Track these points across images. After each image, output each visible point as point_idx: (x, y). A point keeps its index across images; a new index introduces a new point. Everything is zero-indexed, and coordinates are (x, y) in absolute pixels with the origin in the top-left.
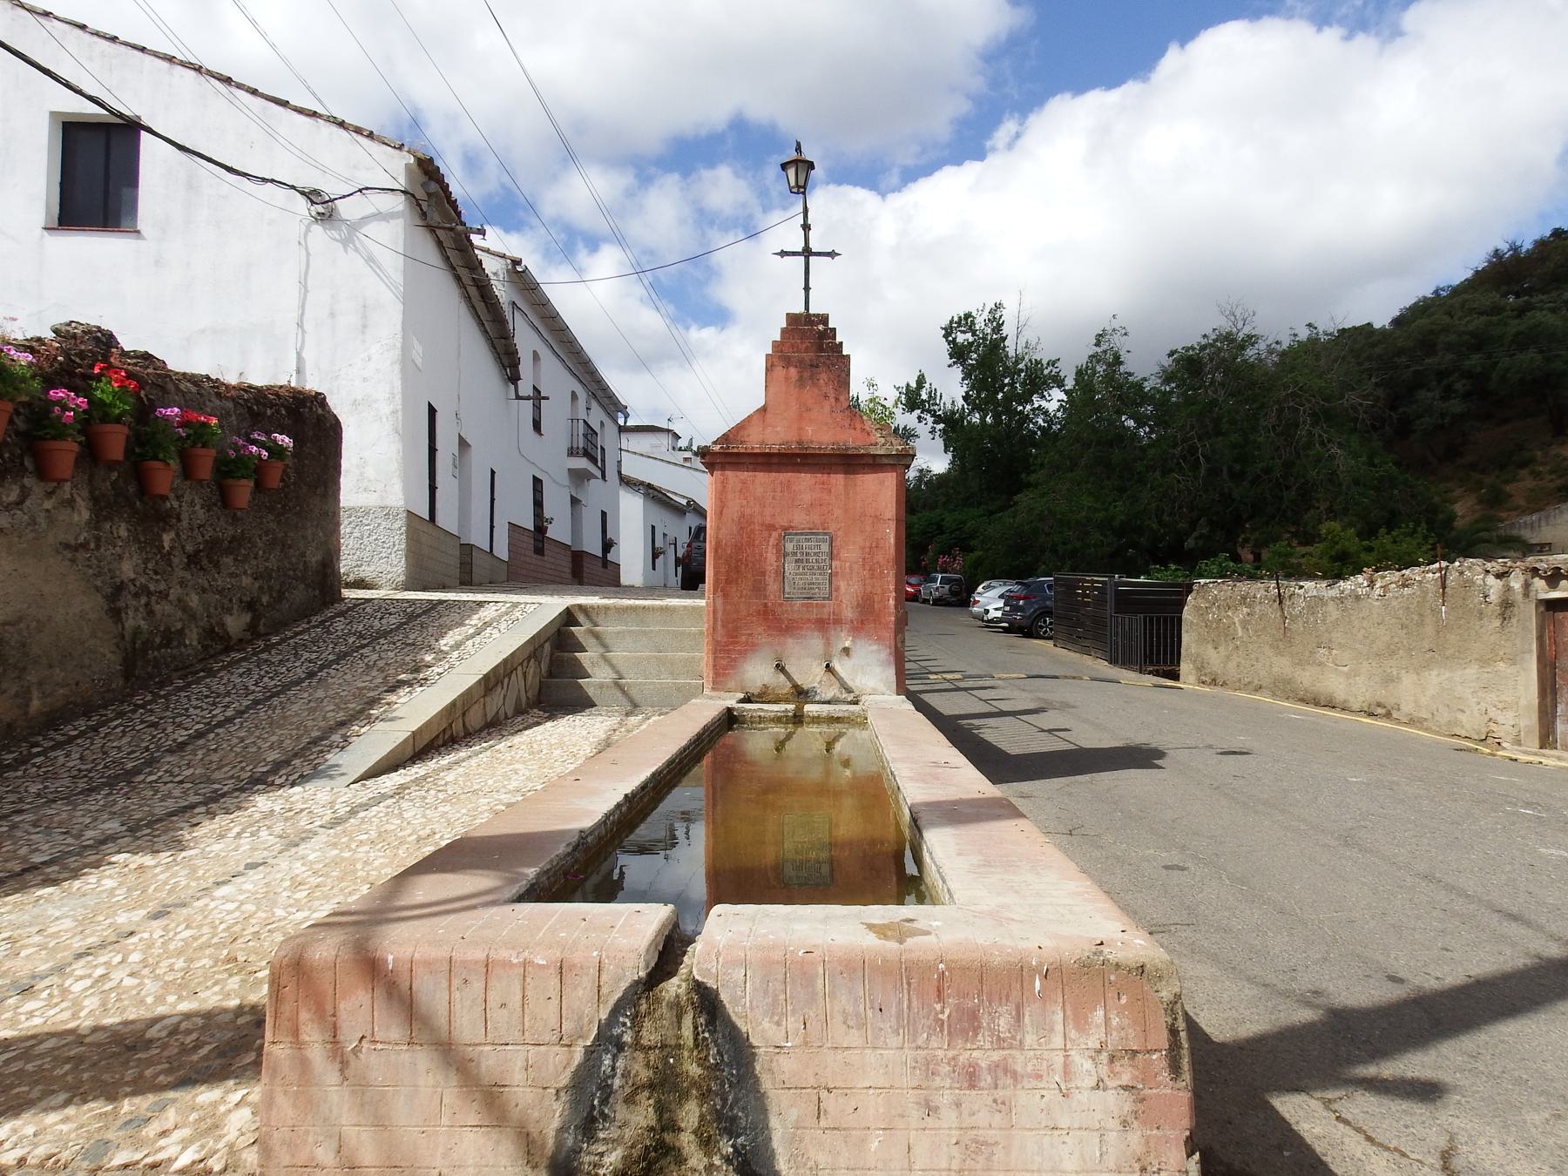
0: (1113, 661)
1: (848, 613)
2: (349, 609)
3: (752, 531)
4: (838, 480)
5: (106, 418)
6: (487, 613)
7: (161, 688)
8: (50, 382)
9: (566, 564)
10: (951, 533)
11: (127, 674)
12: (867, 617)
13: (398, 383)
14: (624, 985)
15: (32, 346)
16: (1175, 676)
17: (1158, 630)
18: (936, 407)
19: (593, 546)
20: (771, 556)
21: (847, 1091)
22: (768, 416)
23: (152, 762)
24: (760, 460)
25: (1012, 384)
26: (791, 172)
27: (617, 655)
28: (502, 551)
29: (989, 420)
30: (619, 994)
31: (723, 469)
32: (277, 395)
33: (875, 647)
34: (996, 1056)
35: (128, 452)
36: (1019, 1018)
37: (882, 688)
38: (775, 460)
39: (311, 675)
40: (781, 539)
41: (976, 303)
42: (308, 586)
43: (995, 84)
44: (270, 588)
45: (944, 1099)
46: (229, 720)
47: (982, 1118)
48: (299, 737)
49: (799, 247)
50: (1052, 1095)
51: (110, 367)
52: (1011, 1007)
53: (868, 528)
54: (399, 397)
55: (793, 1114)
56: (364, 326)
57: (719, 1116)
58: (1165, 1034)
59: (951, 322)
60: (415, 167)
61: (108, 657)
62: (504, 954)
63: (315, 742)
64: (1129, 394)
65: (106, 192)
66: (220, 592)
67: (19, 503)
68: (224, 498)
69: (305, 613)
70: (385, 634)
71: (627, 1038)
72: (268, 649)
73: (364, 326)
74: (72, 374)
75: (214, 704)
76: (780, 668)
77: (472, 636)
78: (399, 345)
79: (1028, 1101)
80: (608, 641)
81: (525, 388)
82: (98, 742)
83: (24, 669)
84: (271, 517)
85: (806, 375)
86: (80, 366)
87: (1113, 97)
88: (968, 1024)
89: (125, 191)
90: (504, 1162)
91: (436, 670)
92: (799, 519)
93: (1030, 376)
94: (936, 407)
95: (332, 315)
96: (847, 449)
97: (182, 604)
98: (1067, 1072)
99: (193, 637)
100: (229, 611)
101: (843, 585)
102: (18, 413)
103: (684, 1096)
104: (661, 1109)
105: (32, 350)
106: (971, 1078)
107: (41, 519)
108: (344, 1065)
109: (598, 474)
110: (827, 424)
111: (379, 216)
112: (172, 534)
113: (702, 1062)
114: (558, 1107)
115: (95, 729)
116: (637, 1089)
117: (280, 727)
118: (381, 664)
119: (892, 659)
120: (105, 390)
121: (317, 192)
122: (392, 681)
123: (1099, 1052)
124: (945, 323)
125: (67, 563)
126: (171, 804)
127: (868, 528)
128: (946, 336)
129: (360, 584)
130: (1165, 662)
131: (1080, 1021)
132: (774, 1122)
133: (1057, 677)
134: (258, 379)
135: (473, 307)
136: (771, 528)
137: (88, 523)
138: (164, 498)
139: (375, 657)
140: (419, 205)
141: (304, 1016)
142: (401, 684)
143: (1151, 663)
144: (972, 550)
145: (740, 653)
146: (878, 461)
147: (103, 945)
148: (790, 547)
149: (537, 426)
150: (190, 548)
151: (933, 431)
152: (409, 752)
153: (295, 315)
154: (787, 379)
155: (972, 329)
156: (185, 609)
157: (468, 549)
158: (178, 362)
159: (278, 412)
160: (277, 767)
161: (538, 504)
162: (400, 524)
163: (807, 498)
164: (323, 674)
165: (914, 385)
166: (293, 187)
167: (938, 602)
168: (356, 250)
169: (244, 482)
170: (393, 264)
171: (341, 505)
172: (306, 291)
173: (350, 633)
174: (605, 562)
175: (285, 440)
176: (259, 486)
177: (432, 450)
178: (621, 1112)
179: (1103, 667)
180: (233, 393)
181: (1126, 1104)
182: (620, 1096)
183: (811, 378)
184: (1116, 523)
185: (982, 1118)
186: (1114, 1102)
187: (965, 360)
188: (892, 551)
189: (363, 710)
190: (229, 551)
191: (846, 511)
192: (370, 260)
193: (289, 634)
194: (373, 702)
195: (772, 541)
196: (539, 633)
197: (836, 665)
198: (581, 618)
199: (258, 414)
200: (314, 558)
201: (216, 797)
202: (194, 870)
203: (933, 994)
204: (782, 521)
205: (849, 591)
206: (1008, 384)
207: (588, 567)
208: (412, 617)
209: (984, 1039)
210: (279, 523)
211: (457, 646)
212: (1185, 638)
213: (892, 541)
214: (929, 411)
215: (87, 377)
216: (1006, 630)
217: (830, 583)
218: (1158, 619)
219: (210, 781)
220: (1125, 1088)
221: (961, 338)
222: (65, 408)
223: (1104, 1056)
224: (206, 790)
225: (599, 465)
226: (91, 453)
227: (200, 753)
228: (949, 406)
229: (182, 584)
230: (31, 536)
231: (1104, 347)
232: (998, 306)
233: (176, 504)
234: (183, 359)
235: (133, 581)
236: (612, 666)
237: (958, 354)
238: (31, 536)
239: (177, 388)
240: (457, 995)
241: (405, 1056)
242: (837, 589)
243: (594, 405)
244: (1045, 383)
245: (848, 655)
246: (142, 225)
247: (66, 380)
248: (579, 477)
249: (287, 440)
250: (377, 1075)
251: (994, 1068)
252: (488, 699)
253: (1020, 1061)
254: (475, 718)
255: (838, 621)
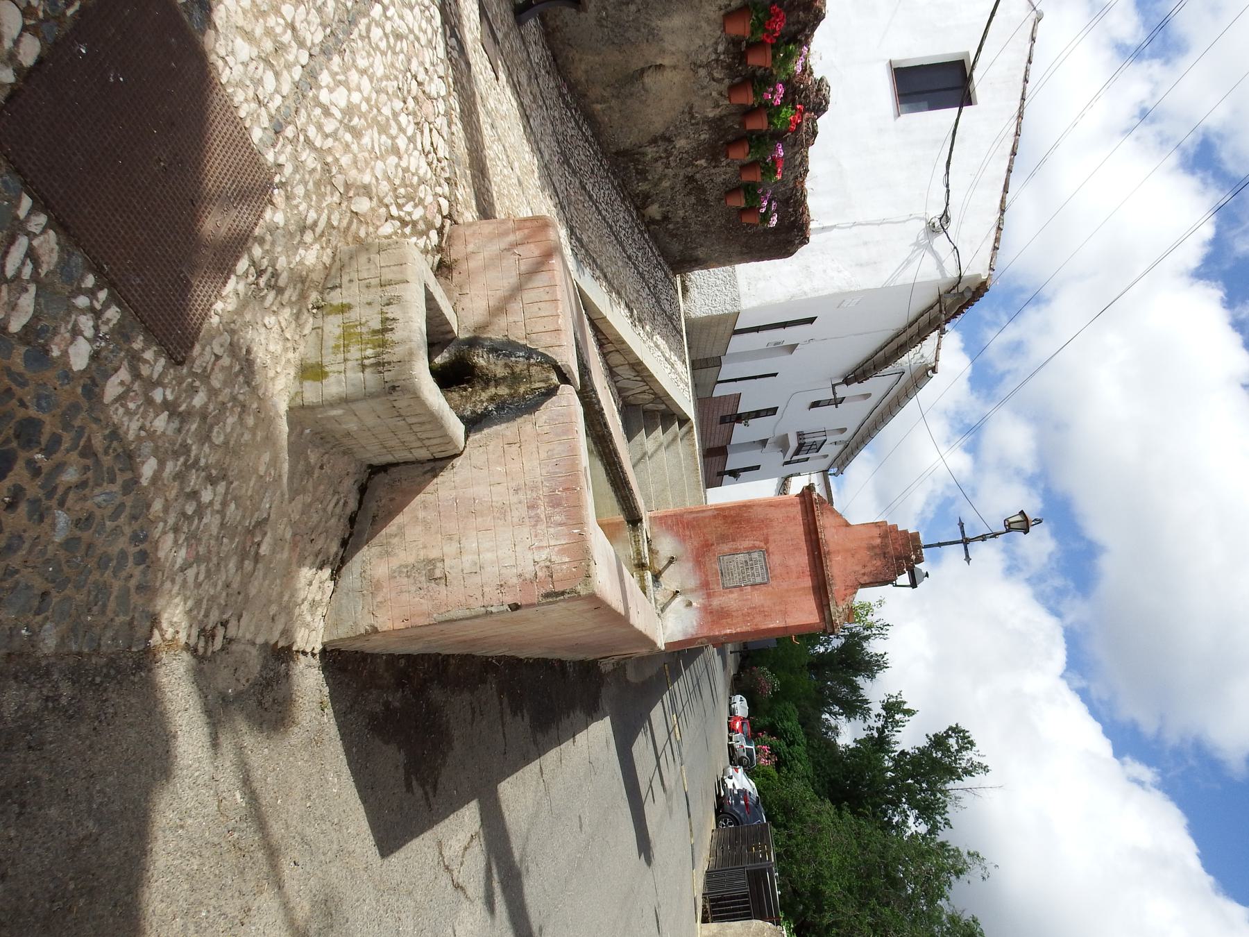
0: (709, 874)
1: (716, 602)
2: (670, 280)
3: (761, 529)
4: (807, 582)
5: (770, 116)
6: (679, 366)
7: (612, 174)
8: (786, 84)
9: (716, 443)
10: (790, 754)
11: (618, 153)
12: (715, 615)
13: (826, 293)
14: (554, 357)
15: (806, 69)
16: (704, 920)
17: (739, 909)
18: (890, 728)
19: (733, 462)
20: (747, 543)
21: (521, 455)
22: (844, 529)
23: (574, 173)
24: (812, 527)
25: (922, 790)
26: (1019, 518)
27: (663, 455)
28: (720, 391)
29: (889, 774)
30: (550, 355)
31: (801, 503)
32: (803, 213)
33: (695, 623)
34: (543, 516)
35: (752, 132)
36: (560, 524)
37: (668, 632)
38: (814, 537)
39: (629, 258)
40: (759, 549)
41: (984, 749)
42: (682, 251)
43: (1178, 753)
44: (678, 229)
45: (522, 496)
46: (600, 213)
47: (516, 514)
48: (596, 252)
49: (968, 535)
50: (529, 542)
51: (802, 114)
52: (565, 521)
53: (777, 608)
54: (817, 295)
55: (508, 433)
56: (861, 265)
57: (504, 402)
58: (562, 589)
59: (964, 731)
60: (980, 281)
61: (627, 142)
62: (560, 306)
63: (594, 261)
64: (933, 889)
65: (922, 93)
66: (672, 198)
67: (714, 80)
68: (732, 191)
69: (664, 253)
70: (658, 301)
71: (532, 361)
72: (641, 232)
73: (861, 265)
74: (794, 93)
75: (607, 204)
76: (671, 560)
77: (664, 356)
78: (852, 289)
79: (525, 532)
80: (672, 448)
81: (842, 391)
82: (581, 143)
83: (618, 97)
84: (723, 221)
85: (877, 551)
86: (800, 97)
87: (1194, 863)
88: (555, 503)
89: (925, 104)
90: (476, 318)
91: (642, 332)
92: (776, 559)
93: (932, 803)
94: (890, 728)
95: (865, 243)
96: (830, 585)
97: (663, 177)
98: (539, 548)
99: (643, 187)
100: (661, 206)
101: (735, 595)
102: (765, 70)
103: (510, 387)
104: (504, 378)
105: (804, 70)
106: (532, 507)
107: (706, 92)
108: (508, 250)
109: (788, 459)
110: (845, 569)
111: (940, 263)
112: (705, 165)
113: (526, 393)
114: (500, 337)
115: (587, 141)
116: (511, 368)
117: (600, 241)
118: (641, 299)
119: (689, 637)
120: (787, 113)
121: (948, 220)
122: (632, 305)
123: (550, 561)
124: (963, 726)
125: (681, 109)
126: (557, 185)
127: (777, 608)
128: (951, 728)
129: (685, 290)
130: (714, 912)
131: (563, 551)
132: (504, 425)
133: (689, 816)
134: (810, 202)
135: (892, 341)
136: (767, 541)
137: (706, 117)
138: (727, 157)
139: (644, 295)
140: (954, 288)
141: (526, 231)
142: (631, 311)
143: (712, 907)
144: (778, 771)
145: (678, 532)
146: (825, 608)
147: (508, 157)
148: (755, 555)
149: (816, 404)
150: (698, 176)
151: (870, 728)
152: (594, 316)
153: (861, 220)
154: (872, 538)
155: (961, 749)
156: (660, 180)
157: (717, 362)
158: (813, 152)
159: (792, 215)
160: (579, 240)
161: (757, 414)
162: (730, 309)
163: (791, 563)
164: (631, 265)
165: (906, 707)
166: (947, 205)
167: (731, 747)
168: (913, 252)
169: (744, 201)
170: (908, 277)
171: (737, 266)
172: (879, 225)
173: (656, 280)
174: (722, 474)
175: (774, 222)
176: (742, 211)
177: (784, 325)
178: (501, 362)
179: (703, 865)
180: (799, 186)
181: (529, 575)
182: (508, 361)
183: (876, 554)
184: (821, 887)
185: (516, 514)
186: (529, 570)
187: (933, 747)
188: (764, 627)
189: (615, 288)
190: (699, 200)
191: (787, 591)
192: (908, 262)
193: (651, 244)
194: (618, 293)
195: (757, 543)
196: (671, 399)
197: (679, 599)
198: (684, 429)
199: (788, 203)
200: (700, 253)
201: (563, 208)
202: (535, 198)
203: (567, 486)
204: (772, 547)
205: (731, 600)
206: (921, 787)
207: (716, 460)
208: (670, 318)
209: (549, 509)
210: (720, 227)
211: (657, 346)
212: (737, 924)
213: (772, 626)
214: (886, 722)
215: (793, 101)
216: (718, 796)
217: (735, 587)
218: (748, 908)
219: (569, 204)
220: (536, 574)
221: (952, 741)
222: (773, 94)
223: (548, 564)
224: (565, 203)
225: (795, 458)
226: (748, 112)
227: (581, 198)
228: (894, 739)
229: (675, 176)
230: (695, 88)
231: (968, 860)
232: (986, 769)
233: (724, 164)
234: (817, 155)
235: (674, 147)
236: (656, 451)
237: (939, 742)
238: (695, 88)
239: (796, 153)
240: (542, 290)
241: (514, 273)
242: (731, 592)
243: (840, 447)
244: (930, 818)
245: (687, 606)
246: (903, 116)
247: (790, 91)
248: (783, 444)
249: (775, 223)
250: (505, 263)
251: (538, 516)
252: (627, 367)
253: (542, 527)
254: (616, 359)
255: (709, 596)
